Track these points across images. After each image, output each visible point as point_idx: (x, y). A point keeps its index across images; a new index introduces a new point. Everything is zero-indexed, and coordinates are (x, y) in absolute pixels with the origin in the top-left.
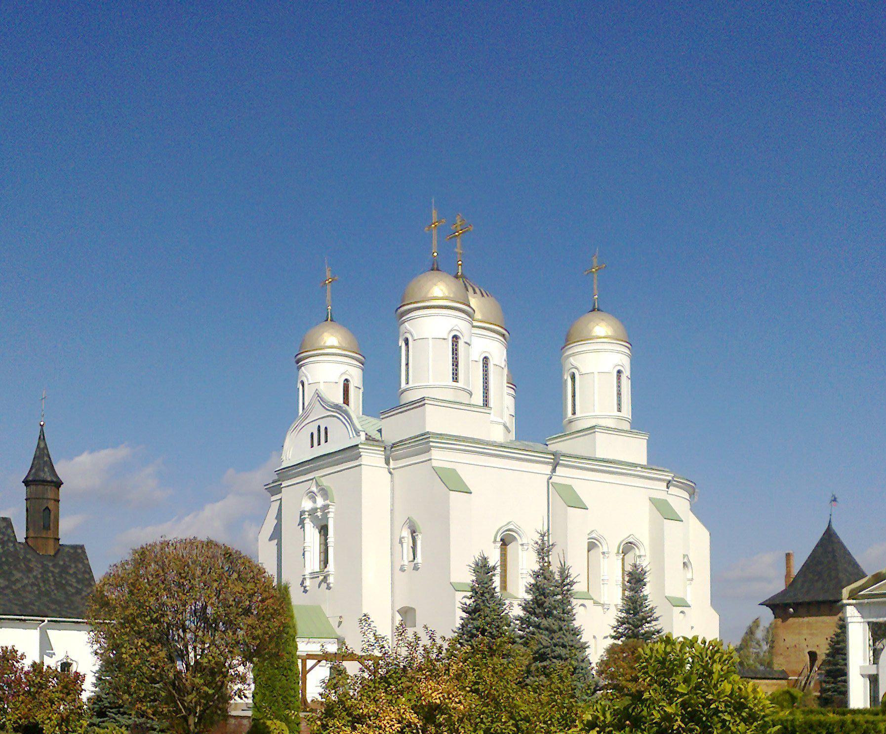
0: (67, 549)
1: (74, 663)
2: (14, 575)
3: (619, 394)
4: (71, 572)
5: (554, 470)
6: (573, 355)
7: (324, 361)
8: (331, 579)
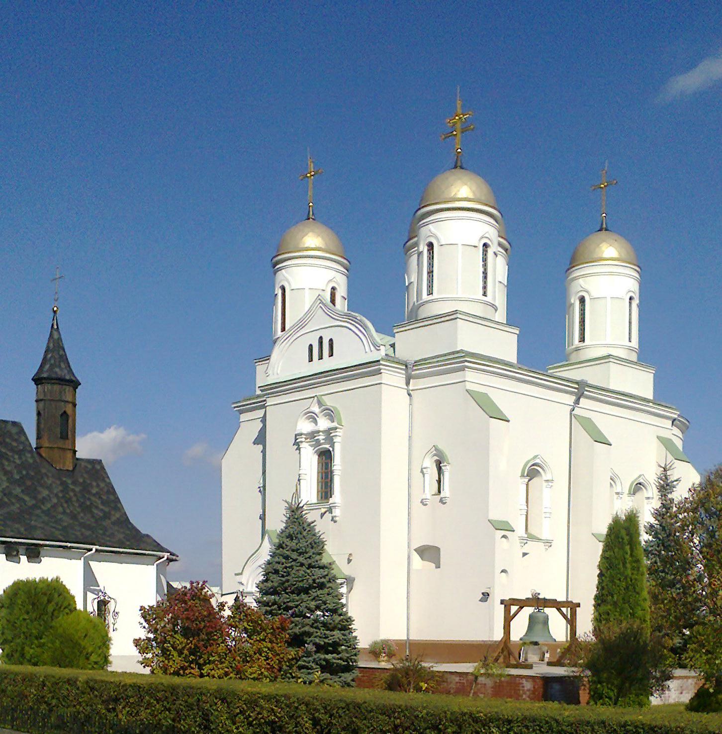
0: (83, 464)
1: (112, 603)
2: (39, 492)
3: (412, 329)
4: (94, 491)
5: (577, 402)
6: (583, 276)
7: (305, 265)
8: (337, 512)
